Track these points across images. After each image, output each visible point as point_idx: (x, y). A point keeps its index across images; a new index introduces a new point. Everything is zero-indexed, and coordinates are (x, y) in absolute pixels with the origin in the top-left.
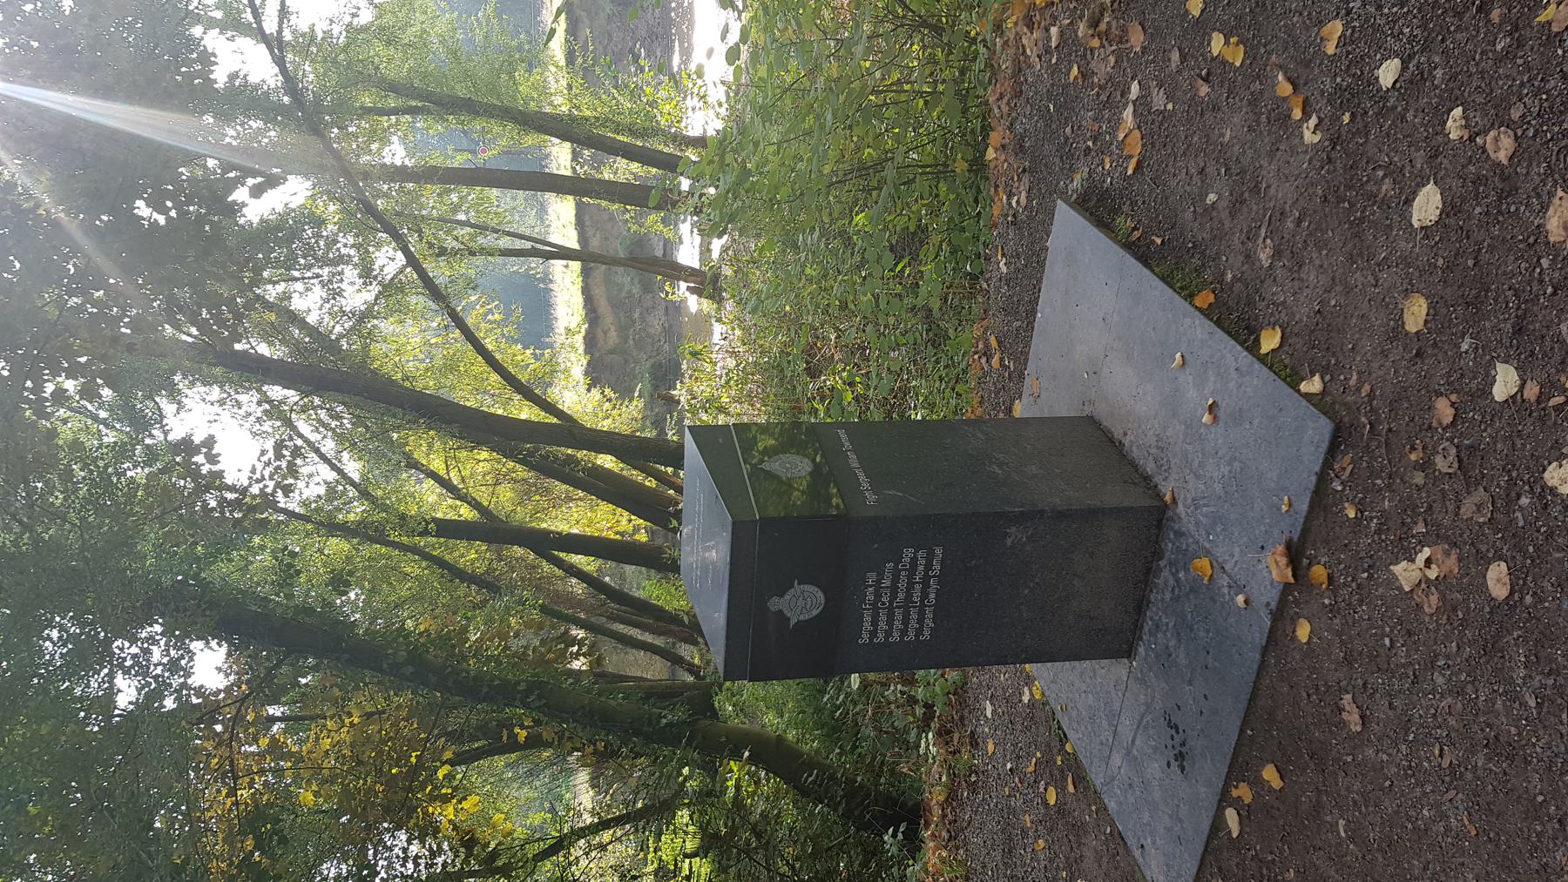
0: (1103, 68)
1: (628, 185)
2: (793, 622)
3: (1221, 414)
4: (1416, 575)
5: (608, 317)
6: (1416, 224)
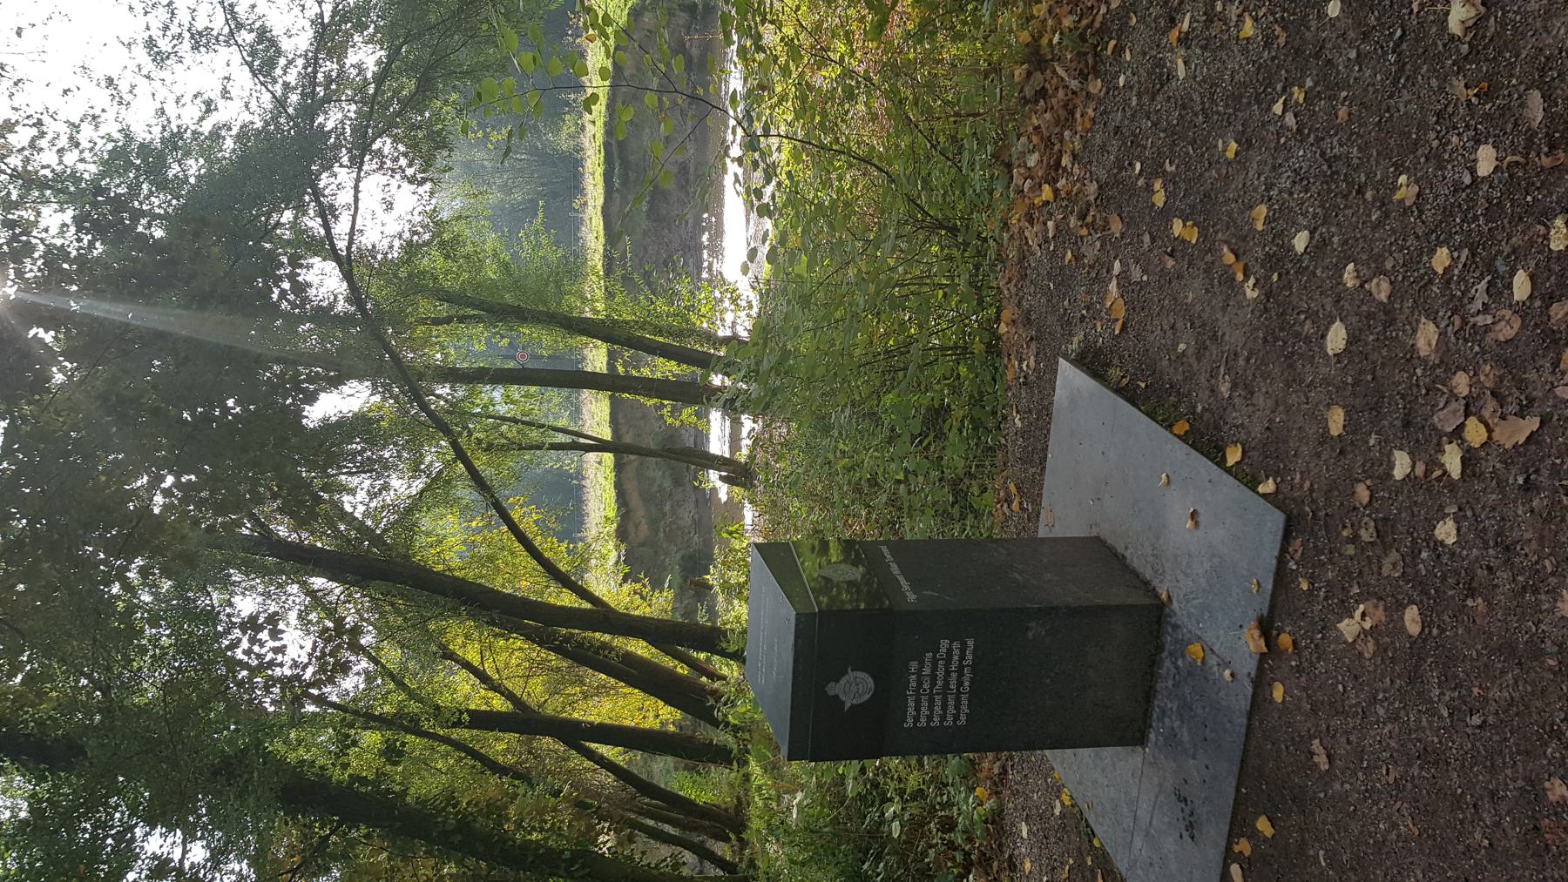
0: (1091, 252)
3: (1201, 519)
5: (640, 512)
6: (1330, 353)
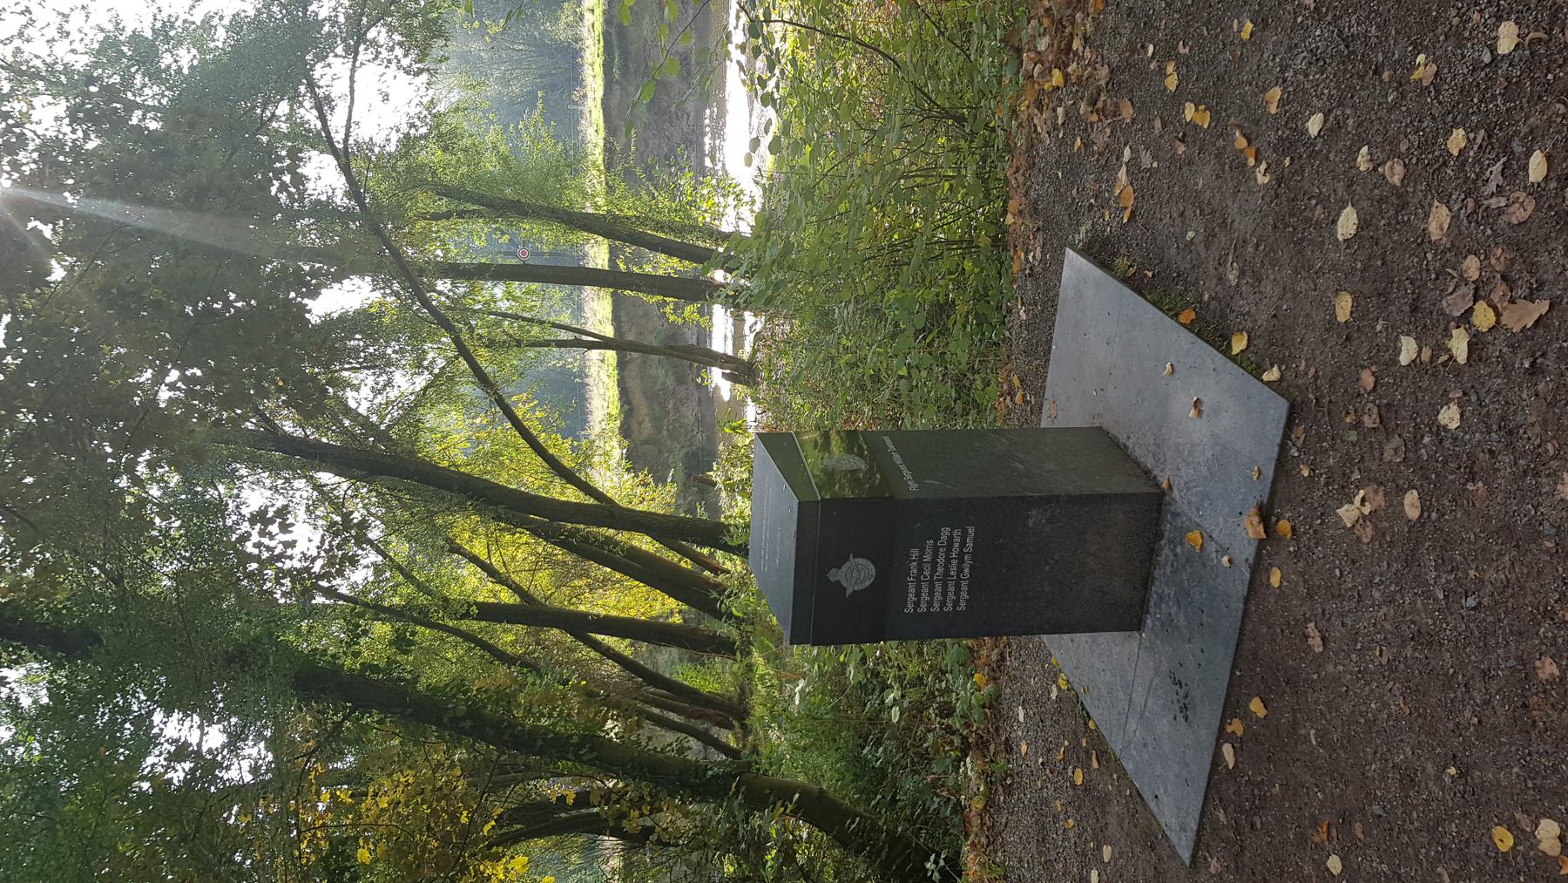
0: (1101, 139)
1: (668, 278)
2: (849, 592)
4: (1355, 514)
5: (643, 410)
